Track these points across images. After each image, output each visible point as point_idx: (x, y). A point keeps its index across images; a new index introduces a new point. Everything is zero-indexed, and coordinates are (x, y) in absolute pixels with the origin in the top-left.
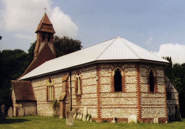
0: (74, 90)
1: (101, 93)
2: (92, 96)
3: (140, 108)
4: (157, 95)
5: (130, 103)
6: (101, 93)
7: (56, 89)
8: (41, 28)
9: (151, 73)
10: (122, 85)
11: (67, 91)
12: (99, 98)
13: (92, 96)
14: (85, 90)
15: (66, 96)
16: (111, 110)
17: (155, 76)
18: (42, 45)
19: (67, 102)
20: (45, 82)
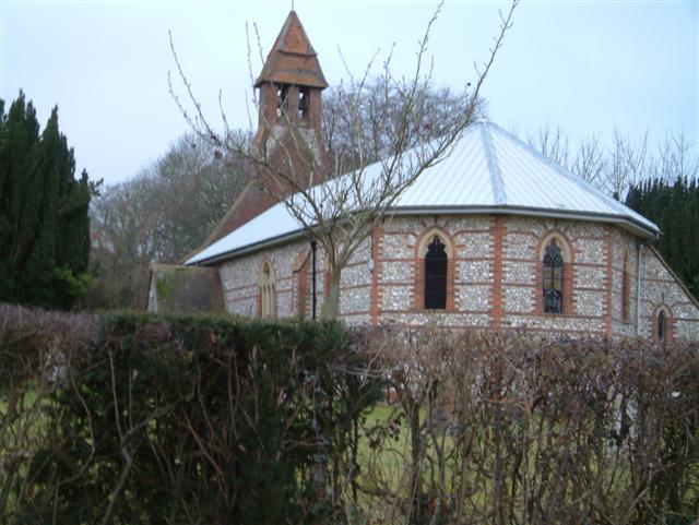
1: (380, 312)
6: (380, 312)
17: (567, 259)
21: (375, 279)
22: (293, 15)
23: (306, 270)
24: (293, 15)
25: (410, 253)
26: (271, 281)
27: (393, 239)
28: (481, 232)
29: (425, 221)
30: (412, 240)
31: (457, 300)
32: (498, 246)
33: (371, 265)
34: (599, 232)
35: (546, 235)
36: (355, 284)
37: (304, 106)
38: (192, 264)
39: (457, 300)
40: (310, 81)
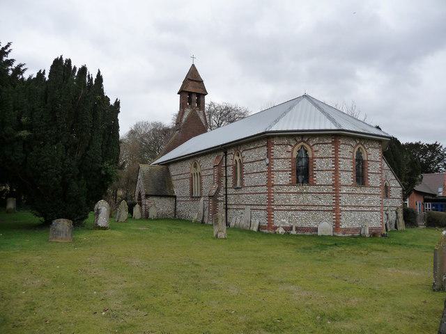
22: (193, 65)
24: (193, 65)
25: (289, 155)
26: (199, 170)
27: (279, 148)
28: (327, 144)
29: (297, 138)
30: (290, 148)
31: (315, 179)
33: (267, 161)
35: (356, 146)
36: (255, 171)
38: (158, 164)
39: (315, 179)
40: (200, 91)
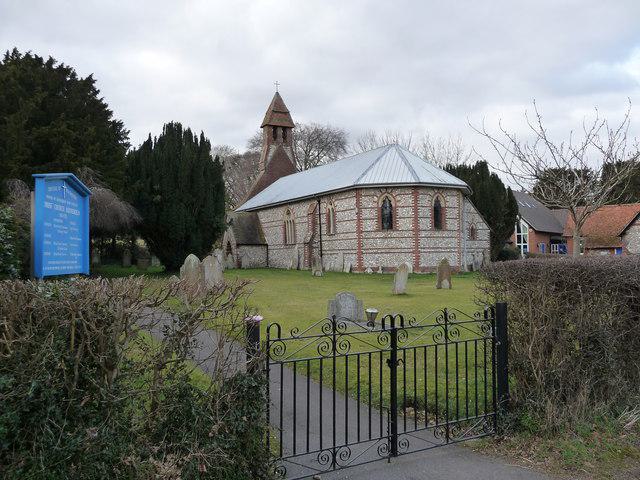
0: (324, 228)
1: (362, 232)
2: (350, 236)
3: (416, 252)
4: (445, 234)
5: (403, 245)
6: (362, 232)
7: (298, 227)
8: (271, 119)
9: (437, 202)
10: (475, 205)
11: (314, 230)
12: (417, 246)
13: (350, 236)
14: (340, 228)
15: (313, 237)
16: (376, 256)
17: (443, 205)
18: (273, 148)
19: (314, 245)
20: (280, 212)
21: (359, 217)
23: (314, 215)
32: (416, 200)
34: (455, 193)
37: (284, 137)
40: (286, 124)
